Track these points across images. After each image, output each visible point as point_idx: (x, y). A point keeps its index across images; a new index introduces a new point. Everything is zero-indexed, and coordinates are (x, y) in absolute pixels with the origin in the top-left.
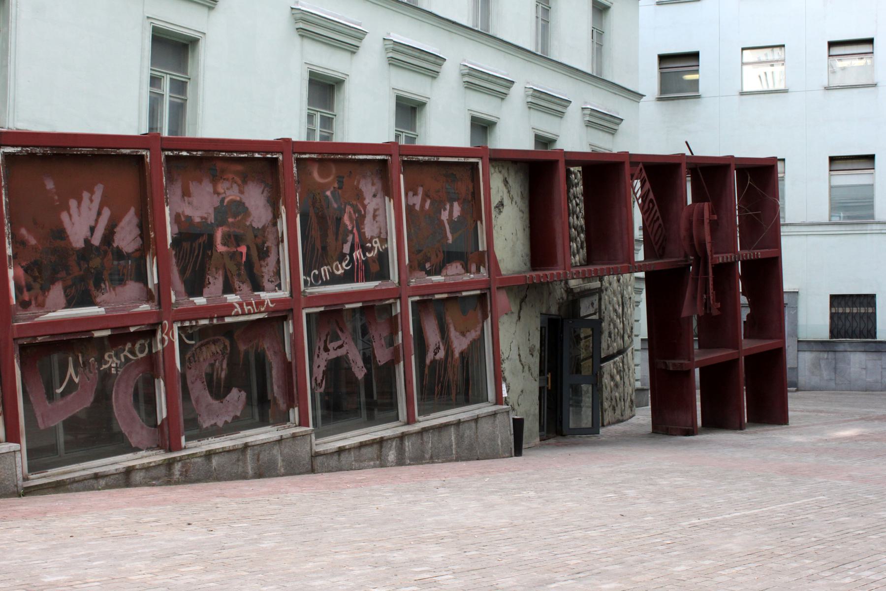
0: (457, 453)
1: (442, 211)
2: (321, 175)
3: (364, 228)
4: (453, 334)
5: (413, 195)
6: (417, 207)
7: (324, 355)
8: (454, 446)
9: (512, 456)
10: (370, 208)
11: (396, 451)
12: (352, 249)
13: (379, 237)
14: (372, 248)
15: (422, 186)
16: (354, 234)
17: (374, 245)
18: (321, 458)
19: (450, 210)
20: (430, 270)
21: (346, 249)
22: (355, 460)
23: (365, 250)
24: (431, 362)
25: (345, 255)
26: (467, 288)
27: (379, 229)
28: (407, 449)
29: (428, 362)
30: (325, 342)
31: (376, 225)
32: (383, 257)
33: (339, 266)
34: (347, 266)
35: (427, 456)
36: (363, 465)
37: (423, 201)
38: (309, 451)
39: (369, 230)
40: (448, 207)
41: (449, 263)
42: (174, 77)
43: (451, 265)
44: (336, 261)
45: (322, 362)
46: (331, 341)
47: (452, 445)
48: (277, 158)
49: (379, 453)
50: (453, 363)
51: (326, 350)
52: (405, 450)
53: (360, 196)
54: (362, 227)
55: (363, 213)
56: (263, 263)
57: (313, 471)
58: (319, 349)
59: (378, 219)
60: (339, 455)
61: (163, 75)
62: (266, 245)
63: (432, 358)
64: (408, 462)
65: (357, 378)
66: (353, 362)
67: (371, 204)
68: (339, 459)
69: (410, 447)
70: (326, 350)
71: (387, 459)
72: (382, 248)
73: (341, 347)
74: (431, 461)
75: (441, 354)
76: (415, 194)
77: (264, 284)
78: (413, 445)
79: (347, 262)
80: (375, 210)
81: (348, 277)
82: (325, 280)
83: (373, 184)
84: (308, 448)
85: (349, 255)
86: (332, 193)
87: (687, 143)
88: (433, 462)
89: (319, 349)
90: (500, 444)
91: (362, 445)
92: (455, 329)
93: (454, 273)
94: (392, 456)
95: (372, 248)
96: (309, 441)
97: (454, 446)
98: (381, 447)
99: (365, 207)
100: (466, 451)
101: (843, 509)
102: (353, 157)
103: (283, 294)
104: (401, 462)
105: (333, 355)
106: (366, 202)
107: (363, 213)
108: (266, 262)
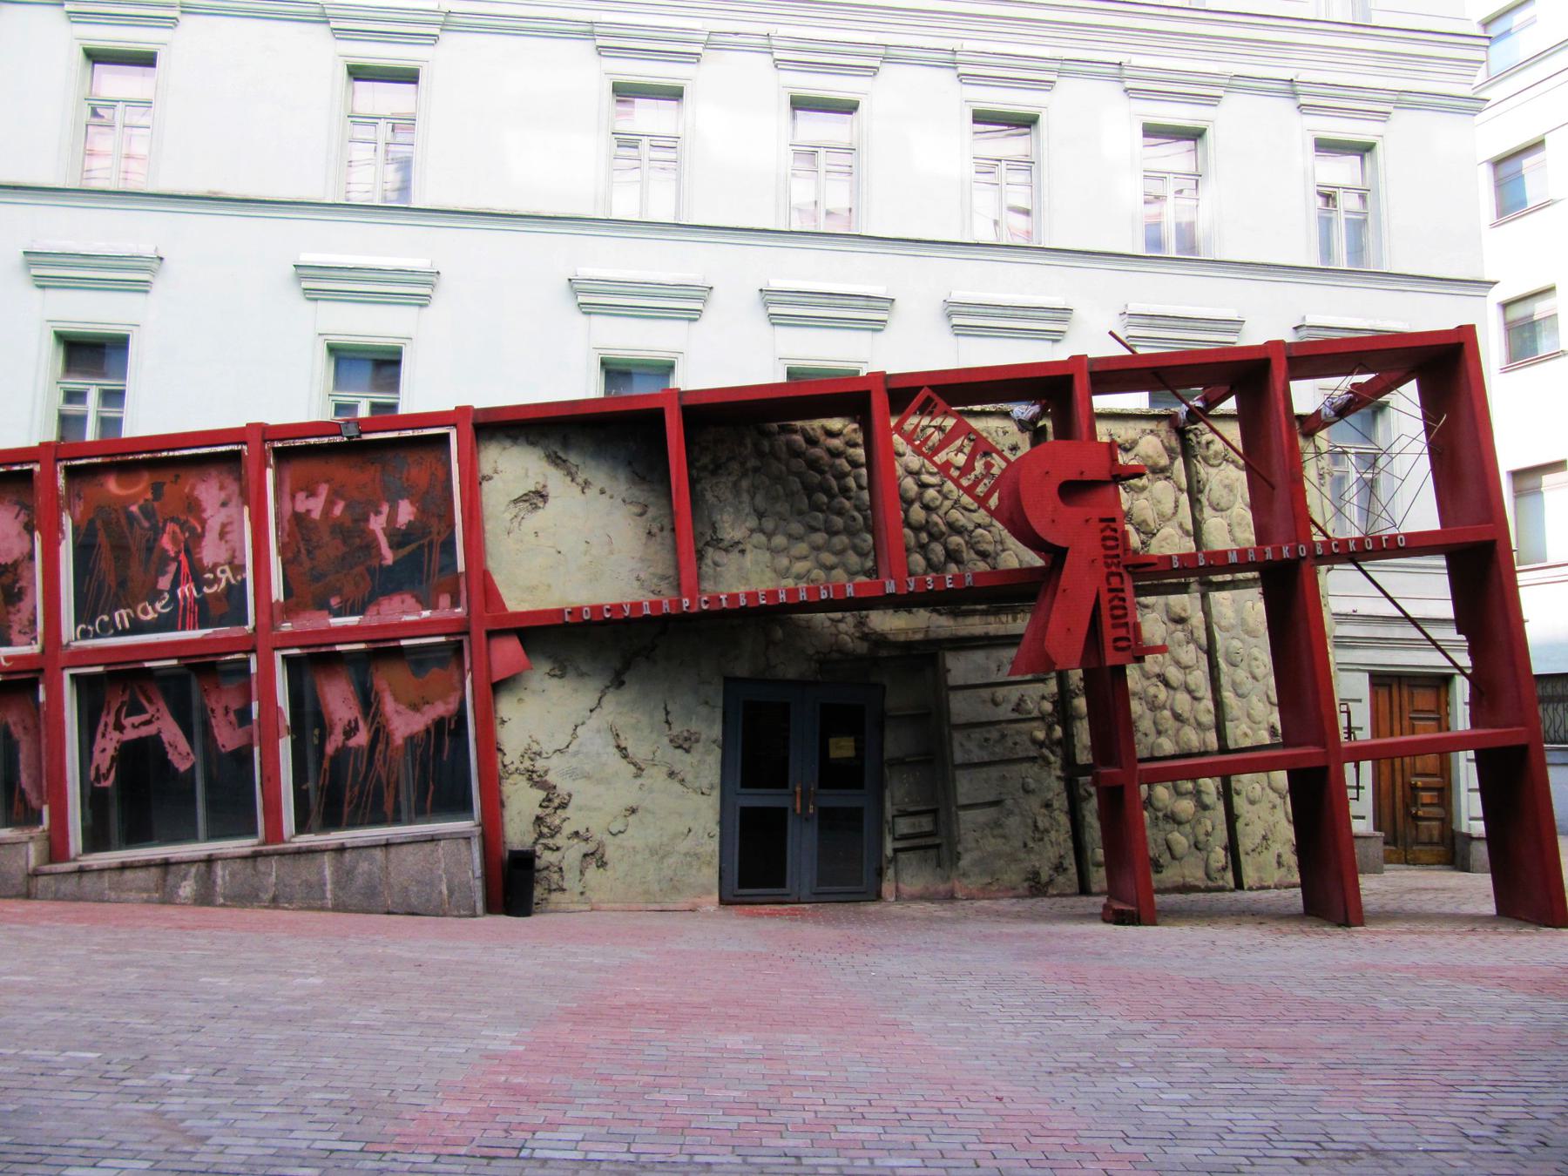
0: (336, 897)
1: (372, 515)
2: (120, 485)
3: (200, 553)
4: (389, 705)
5: (307, 497)
6: (316, 515)
7: (116, 735)
8: (329, 887)
9: (474, 916)
10: (214, 525)
11: (196, 882)
12: (176, 583)
13: (230, 563)
14: (217, 580)
15: (327, 481)
16: (180, 563)
17: (219, 574)
18: (45, 878)
19: (389, 516)
20: (341, 608)
21: (164, 583)
22: (110, 888)
23: (199, 583)
24: (337, 750)
25: (161, 592)
26: (410, 633)
27: (230, 552)
28: (219, 881)
29: (330, 749)
30: (118, 712)
31: (223, 545)
32: (235, 591)
33: (150, 608)
34: (163, 607)
35: (266, 897)
36: (124, 896)
37: (330, 504)
38: (25, 867)
39: (211, 552)
40: (385, 509)
41: (383, 594)
42: (106, 388)
43: (391, 599)
44: (144, 600)
45: (108, 744)
46: (128, 715)
47: (325, 884)
48: (31, 471)
49: (160, 882)
50: (388, 753)
51: (119, 727)
52: (214, 882)
53: (194, 507)
54: (198, 550)
55: (199, 530)
56: (12, 609)
57: (28, 896)
58: (106, 725)
59: (229, 537)
60: (80, 877)
61: (87, 387)
62: (18, 585)
63: (340, 744)
64: (221, 901)
65: (177, 770)
66: (171, 745)
67: (215, 518)
68: (79, 883)
69: (227, 878)
70: (119, 727)
71: (177, 893)
72: (235, 579)
73: (148, 722)
74: (272, 905)
75: (362, 738)
76: (312, 494)
77: (12, 637)
78: (233, 875)
79: (164, 602)
80: (224, 526)
81: (161, 625)
82: (120, 628)
83: (222, 488)
84: (22, 863)
85: (168, 592)
86: (141, 508)
87: (1111, 333)
88: (277, 908)
89: (106, 725)
90: (445, 891)
91: (124, 867)
92: (397, 700)
93: (403, 611)
94: (187, 889)
95: (217, 580)
96: (23, 853)
97: (329, 887)
98: (166, 874)
99: (203, 522)
100: (360, 897)
101: (1004, 1089)
102: (171, 454)
103: (36, 648)
104: (204, 898)
105: (130, 734)
106: (205, 515)
107: (199, 530)
108: (17, 608)
